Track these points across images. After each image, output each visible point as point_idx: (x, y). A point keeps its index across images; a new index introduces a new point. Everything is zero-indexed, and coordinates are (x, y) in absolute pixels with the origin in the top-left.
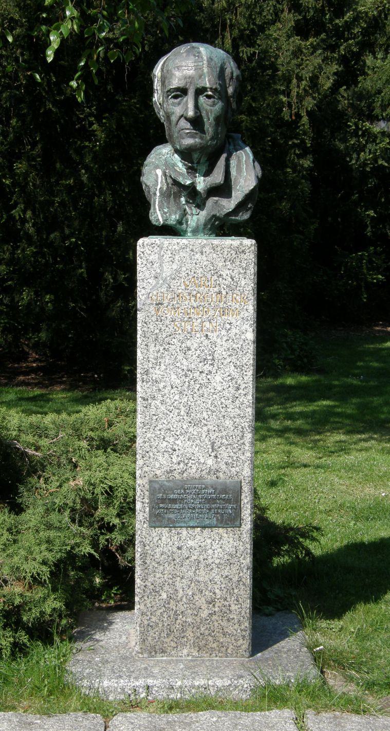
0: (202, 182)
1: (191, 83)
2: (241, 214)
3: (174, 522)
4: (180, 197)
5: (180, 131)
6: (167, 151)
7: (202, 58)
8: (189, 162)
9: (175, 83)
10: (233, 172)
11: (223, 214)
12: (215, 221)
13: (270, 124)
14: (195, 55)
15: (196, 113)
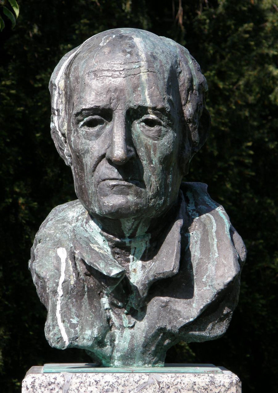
0: (139, 269)
1: (118, 99)
2: (210, 326)
4: (100, 296)
5: (99, 182)
6: (75, 215)
7: (137, 55)
8: (115, 236)
9: (91, 100)
10: (195, 251)
11: (179, 326)
12: (163, 339)
13: (251, 115)
14: (124, 51)
15: (128, 151)
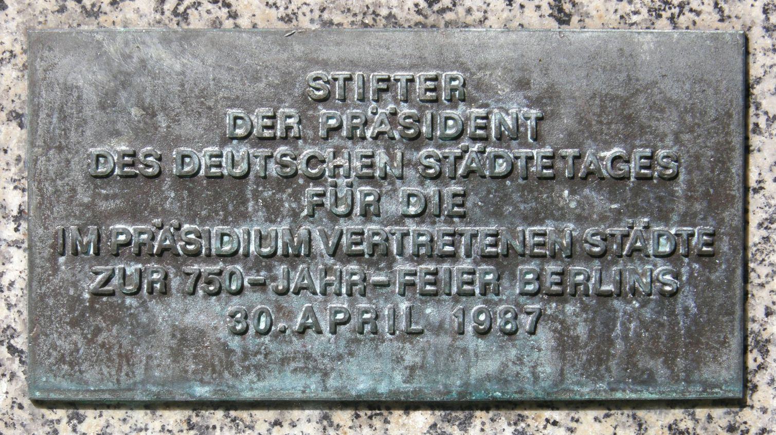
3: (221, 362)
